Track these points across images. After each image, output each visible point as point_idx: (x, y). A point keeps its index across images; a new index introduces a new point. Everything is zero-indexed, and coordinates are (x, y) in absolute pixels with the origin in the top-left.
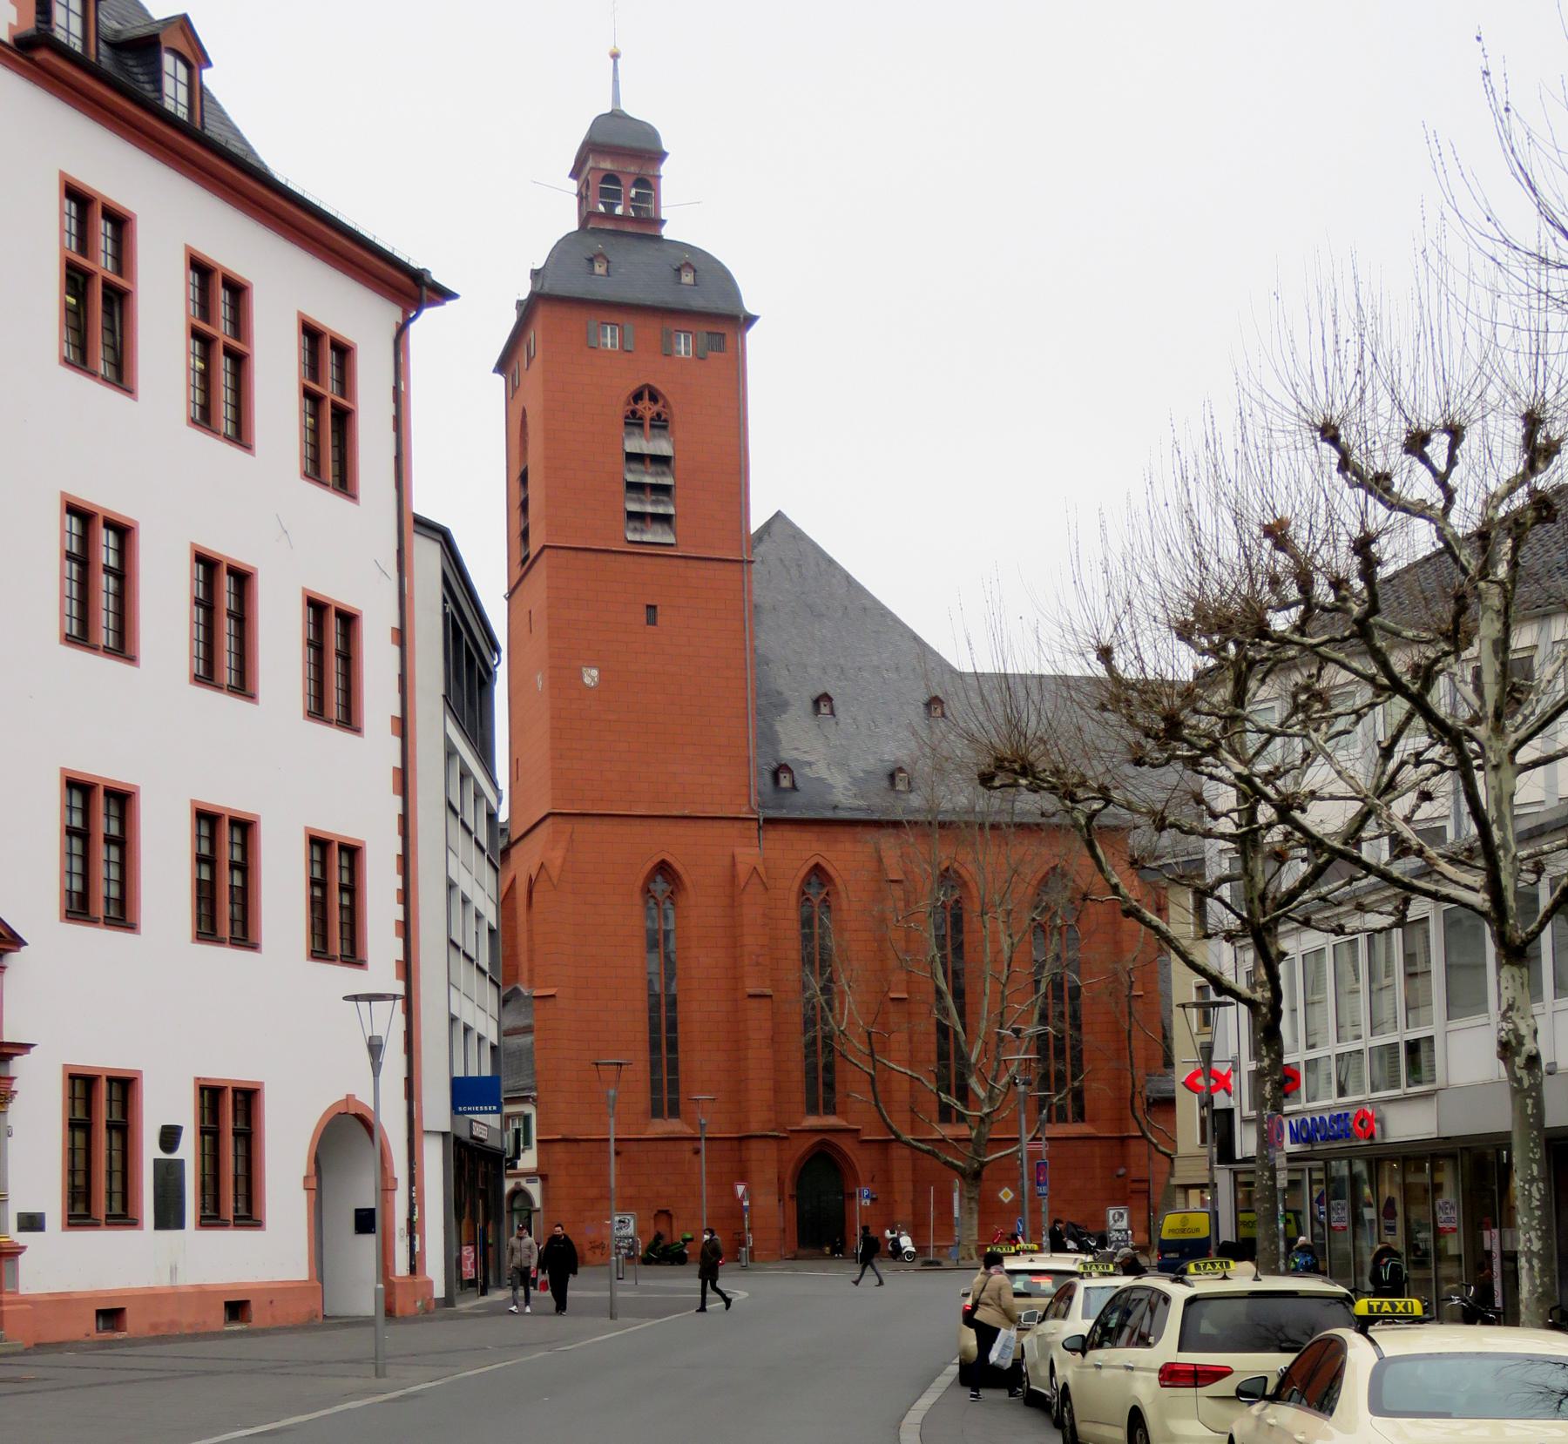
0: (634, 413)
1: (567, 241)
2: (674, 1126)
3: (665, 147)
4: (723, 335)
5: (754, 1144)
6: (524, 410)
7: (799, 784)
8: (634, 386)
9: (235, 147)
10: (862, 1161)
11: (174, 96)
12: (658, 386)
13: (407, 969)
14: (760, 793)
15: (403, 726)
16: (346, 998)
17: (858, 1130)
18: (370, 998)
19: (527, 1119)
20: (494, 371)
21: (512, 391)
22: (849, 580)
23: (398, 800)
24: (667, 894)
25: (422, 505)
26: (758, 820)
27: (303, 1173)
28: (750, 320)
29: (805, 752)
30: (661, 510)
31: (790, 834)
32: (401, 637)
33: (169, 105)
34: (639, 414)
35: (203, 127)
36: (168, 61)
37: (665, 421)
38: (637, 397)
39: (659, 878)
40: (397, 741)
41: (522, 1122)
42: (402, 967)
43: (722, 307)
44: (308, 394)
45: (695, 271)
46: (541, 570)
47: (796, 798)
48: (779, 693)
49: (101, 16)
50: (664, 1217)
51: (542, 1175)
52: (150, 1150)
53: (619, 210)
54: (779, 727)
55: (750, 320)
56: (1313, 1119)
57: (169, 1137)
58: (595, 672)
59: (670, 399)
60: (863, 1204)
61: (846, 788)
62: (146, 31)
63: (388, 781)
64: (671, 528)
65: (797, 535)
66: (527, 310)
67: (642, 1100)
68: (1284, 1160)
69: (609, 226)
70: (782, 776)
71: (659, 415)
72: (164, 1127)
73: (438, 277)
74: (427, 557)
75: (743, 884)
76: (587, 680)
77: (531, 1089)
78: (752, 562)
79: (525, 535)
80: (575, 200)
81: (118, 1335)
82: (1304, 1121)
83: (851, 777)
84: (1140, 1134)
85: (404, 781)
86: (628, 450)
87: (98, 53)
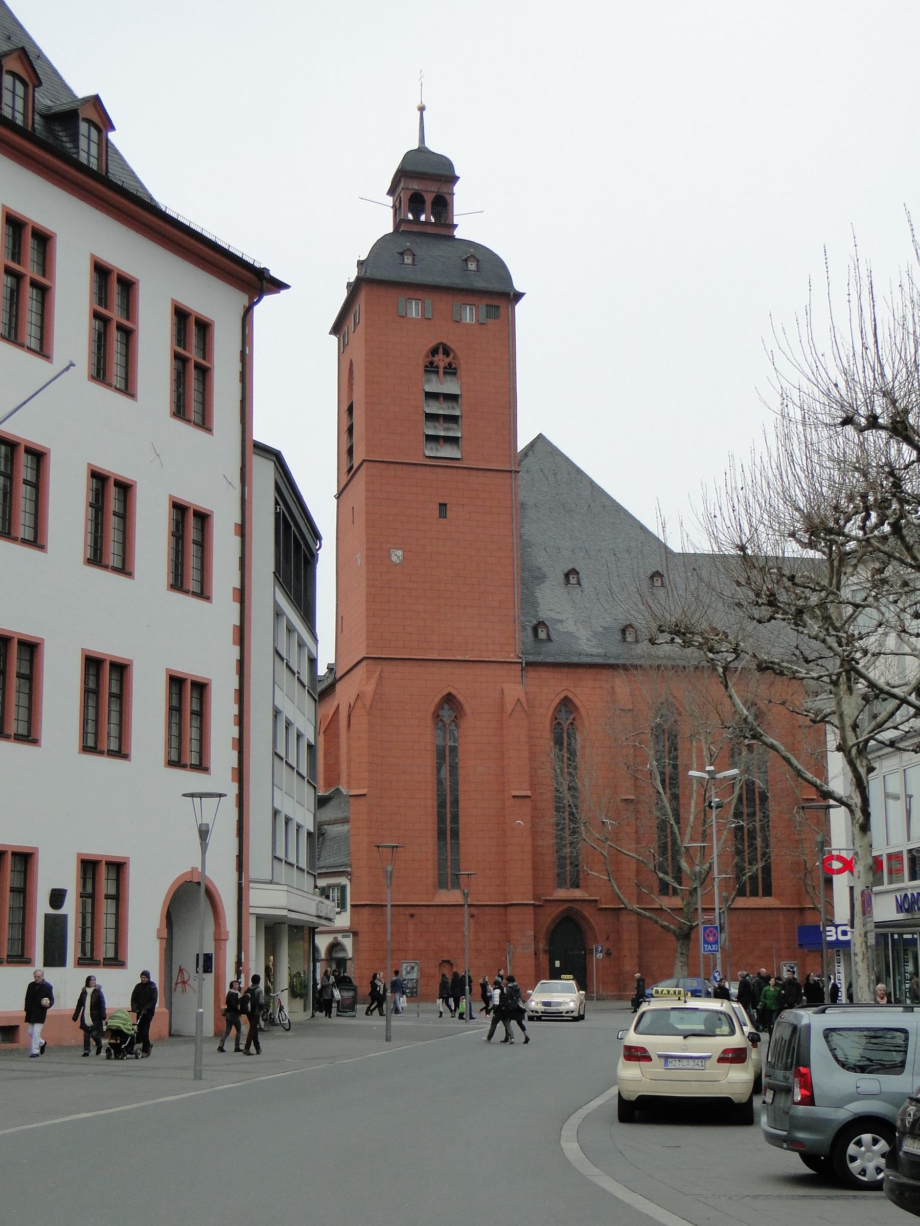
0: (431, 363)
1: (382, 244)
2: (452, 896)
3: (457, 173)
4: (499, 307)
5: (512, 909)
6: (351, 361)
7: (553, 637)
8: (432, 344)
9: (129, 185)
10: (597, 922)
11: (87, 152)
12: (450, 344)
13: (240, 775)
14: (524, 643)
15: (242, 595)
16: (184, 795)
17: (596, 901)
18: (201, 796)
19: (343, 889)
20: (330, 333)
21: (343, 348)
22: (592, 484)
23: (236, 649)
24: (453, 718)
25: (260, 435)
26: (522, 663)
27: (157, 926)
28: (519, 296)
29: (558, 613)
30: (451, 434)
31: (544, 674)
32: (242, 530)
33: (83, 158)
34: (435, 364)
35: (107, 172)
36: (83, 127)
37: (455, 369)
38: (434, 352)
39: (446, 706)
40: (237, 606)
41: (339, 891)
42: (237, 772)
43: (497, 287)
44: (177, 357)
45: (478, 261)
46: (361, 478)
47: (550, 647)
48: (539, 569)
49: (36, 94)
50: (448, 966)
51: (354, 933)
52: (42, 907)
53: (423, 218)
54: (538, 594)
55: (519, 296)
56: (913, 895)
57: (57, 898)
58: (400, 553)
59: (457, 352)
60: (598, 957)
61: (588, 640)
62: (63, 108)
63: (229, 635)
64: (458, 447)
65: (554, 452)
66: (354, 289)
67: (430, 873)
68: (873, 924)
69: (415, 229)
70: (540, 630)
71: (450, 364)
72: (53, 890)
73: (274, 273)
74: (263, 472)
75: (510, 711)
76: (394, 559)
77: (346, 865)
78: (518, 472)
79: (350, 451)
80: (391, 211)
81: (14, 1046)
82: (906, 895)
83: (592, 631)
84: (812, 906)
85: (241, 635)
86: (426, 391)
87: (33, 123)
